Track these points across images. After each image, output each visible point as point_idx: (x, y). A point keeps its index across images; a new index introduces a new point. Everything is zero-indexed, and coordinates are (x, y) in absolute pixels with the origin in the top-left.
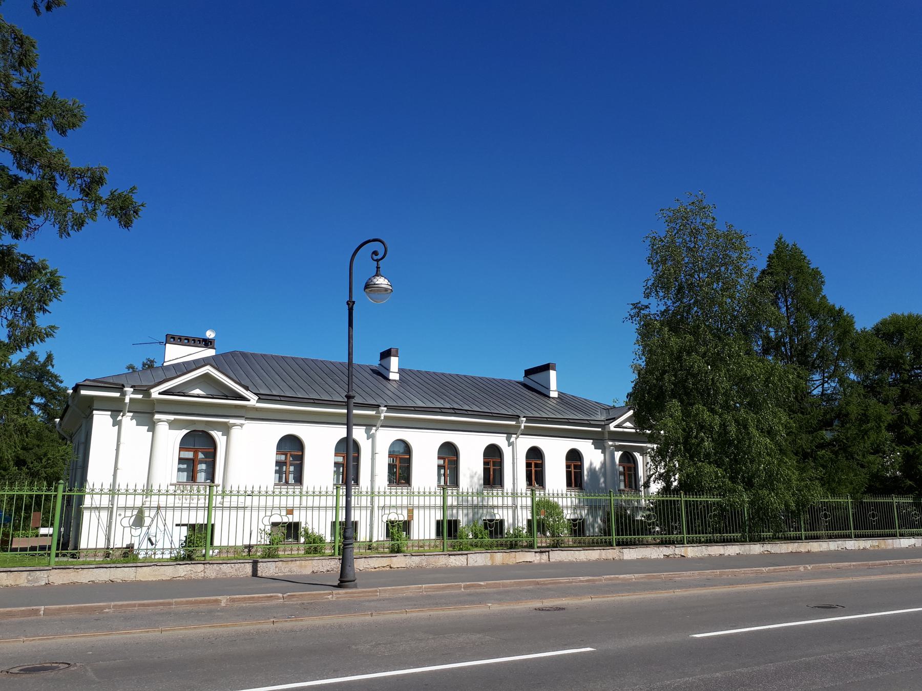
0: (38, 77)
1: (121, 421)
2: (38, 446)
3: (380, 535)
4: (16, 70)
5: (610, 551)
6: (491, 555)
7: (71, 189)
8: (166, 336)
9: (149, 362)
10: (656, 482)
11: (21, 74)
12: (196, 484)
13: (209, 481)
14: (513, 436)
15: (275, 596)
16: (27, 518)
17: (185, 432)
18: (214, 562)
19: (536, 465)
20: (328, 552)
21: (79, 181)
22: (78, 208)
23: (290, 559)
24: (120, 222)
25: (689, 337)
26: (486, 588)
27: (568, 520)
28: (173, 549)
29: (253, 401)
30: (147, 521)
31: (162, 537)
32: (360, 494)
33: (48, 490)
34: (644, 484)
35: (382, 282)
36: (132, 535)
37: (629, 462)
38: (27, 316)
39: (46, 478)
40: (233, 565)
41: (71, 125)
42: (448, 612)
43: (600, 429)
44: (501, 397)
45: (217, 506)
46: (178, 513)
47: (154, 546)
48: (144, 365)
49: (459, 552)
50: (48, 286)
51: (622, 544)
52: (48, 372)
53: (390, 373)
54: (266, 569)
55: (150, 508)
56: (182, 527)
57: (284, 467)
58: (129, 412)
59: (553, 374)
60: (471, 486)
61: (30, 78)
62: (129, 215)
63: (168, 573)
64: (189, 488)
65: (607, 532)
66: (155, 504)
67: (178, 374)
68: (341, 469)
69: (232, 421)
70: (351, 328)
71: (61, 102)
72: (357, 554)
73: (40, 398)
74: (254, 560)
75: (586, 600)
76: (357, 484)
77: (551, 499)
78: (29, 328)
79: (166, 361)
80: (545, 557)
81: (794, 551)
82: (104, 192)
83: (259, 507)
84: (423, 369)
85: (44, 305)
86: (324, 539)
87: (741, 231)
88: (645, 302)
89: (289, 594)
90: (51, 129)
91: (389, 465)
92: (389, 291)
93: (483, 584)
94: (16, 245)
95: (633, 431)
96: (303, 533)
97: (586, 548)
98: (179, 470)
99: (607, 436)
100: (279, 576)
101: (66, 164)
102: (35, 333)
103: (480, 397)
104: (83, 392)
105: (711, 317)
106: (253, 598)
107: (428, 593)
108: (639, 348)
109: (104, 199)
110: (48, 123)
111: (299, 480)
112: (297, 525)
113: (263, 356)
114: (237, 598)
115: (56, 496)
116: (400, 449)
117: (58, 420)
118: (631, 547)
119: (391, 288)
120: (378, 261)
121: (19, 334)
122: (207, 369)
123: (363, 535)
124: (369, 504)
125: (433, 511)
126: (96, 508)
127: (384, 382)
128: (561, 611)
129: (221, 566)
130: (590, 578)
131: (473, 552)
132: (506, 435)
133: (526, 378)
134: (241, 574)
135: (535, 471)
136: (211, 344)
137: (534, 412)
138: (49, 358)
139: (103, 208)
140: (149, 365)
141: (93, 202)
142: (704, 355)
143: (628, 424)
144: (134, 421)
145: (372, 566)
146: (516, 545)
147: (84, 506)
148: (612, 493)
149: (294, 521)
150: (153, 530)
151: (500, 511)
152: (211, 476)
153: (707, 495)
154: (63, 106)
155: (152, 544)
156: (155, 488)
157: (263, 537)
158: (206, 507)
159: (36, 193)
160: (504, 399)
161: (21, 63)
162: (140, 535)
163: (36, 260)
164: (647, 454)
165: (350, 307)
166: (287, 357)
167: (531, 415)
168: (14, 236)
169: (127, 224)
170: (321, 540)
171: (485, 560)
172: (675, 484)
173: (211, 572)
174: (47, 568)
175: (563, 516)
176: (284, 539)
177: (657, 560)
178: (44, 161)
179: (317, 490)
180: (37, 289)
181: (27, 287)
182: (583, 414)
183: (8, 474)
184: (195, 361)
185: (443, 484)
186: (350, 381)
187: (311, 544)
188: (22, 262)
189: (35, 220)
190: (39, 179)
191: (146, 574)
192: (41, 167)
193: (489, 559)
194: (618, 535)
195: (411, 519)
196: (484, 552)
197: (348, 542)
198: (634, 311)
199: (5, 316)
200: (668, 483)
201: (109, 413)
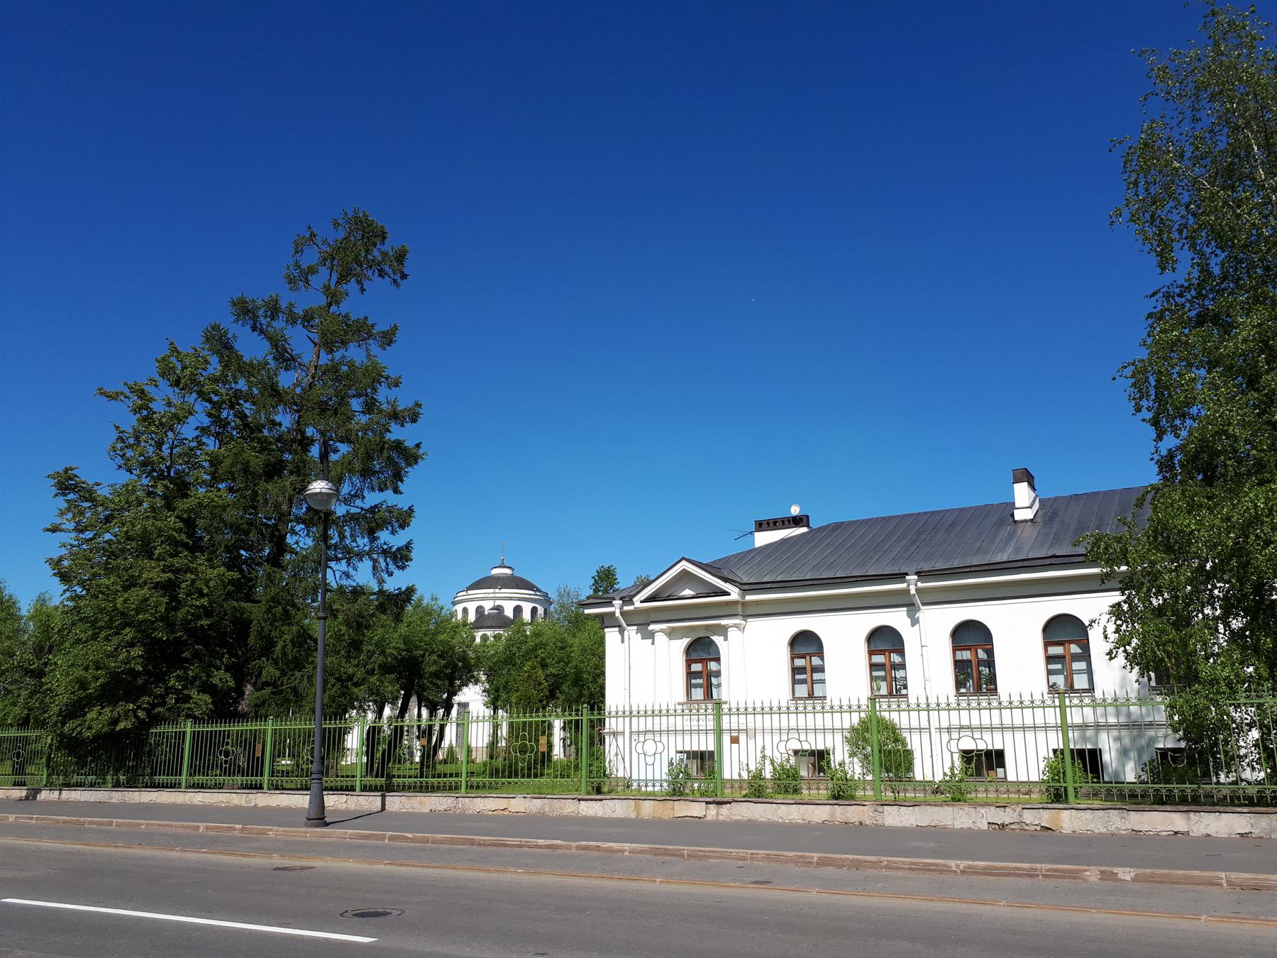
6: (635, 802)
17: (685, 641)
29: (735, 594)
36: (646, 764)
60: (1123, 686)
64: (704, 707)
69: (723, 622)
83: (780, 730)
87: (1122, 157)
125: (1041, 735)
149: (818, 748)
158: (1059, 727)
171: (627, 810)
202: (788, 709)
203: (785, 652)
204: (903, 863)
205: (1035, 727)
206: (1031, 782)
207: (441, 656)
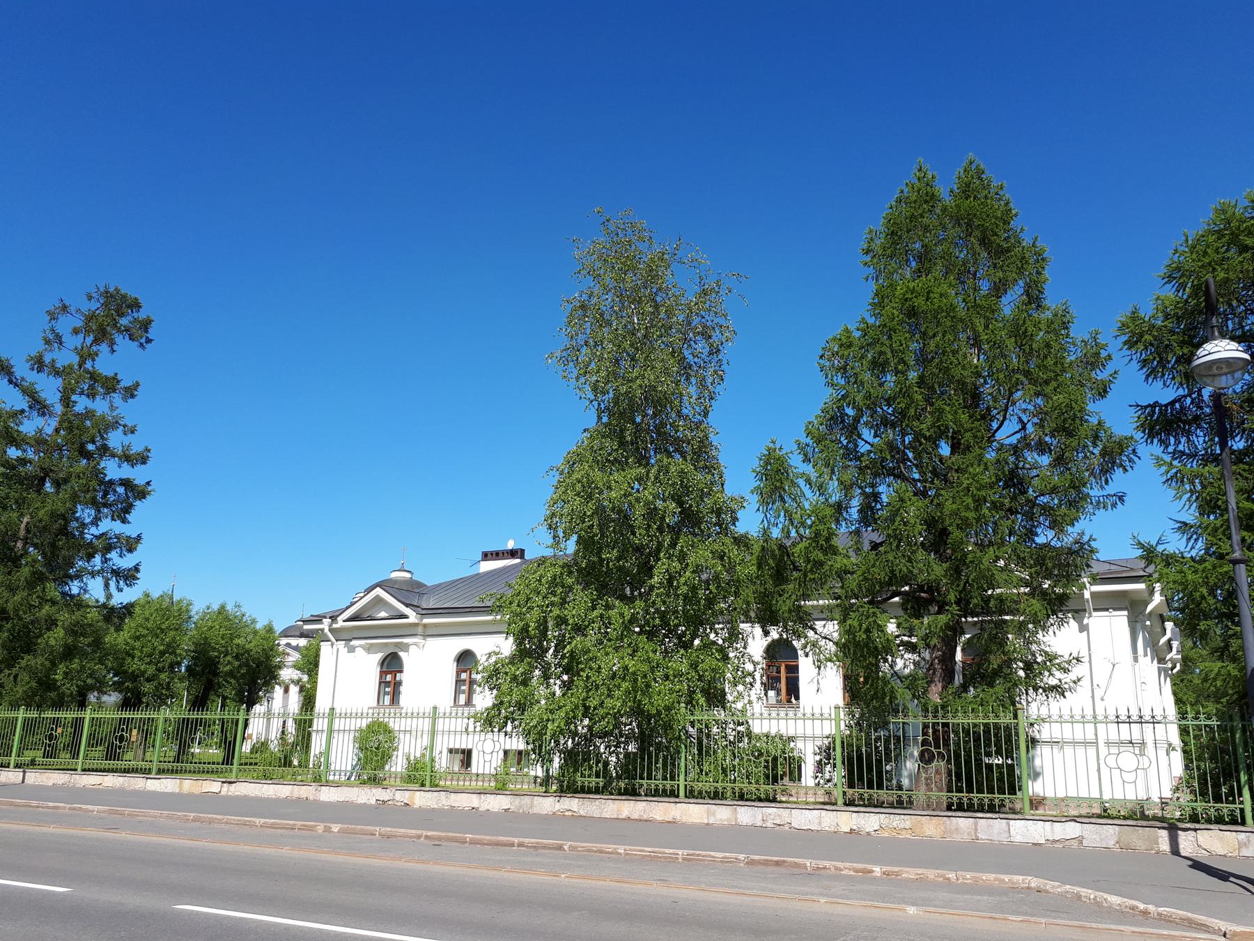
17: (378, 657)
29: (413, 617)
36: (1124, 781)
69: (406, 640)
81: (635, 816)
153: (122, 711)
177: (364, 806)
202: (761, 715)
203: (452, 668)
204: (234, 820)
207: (237, 657)
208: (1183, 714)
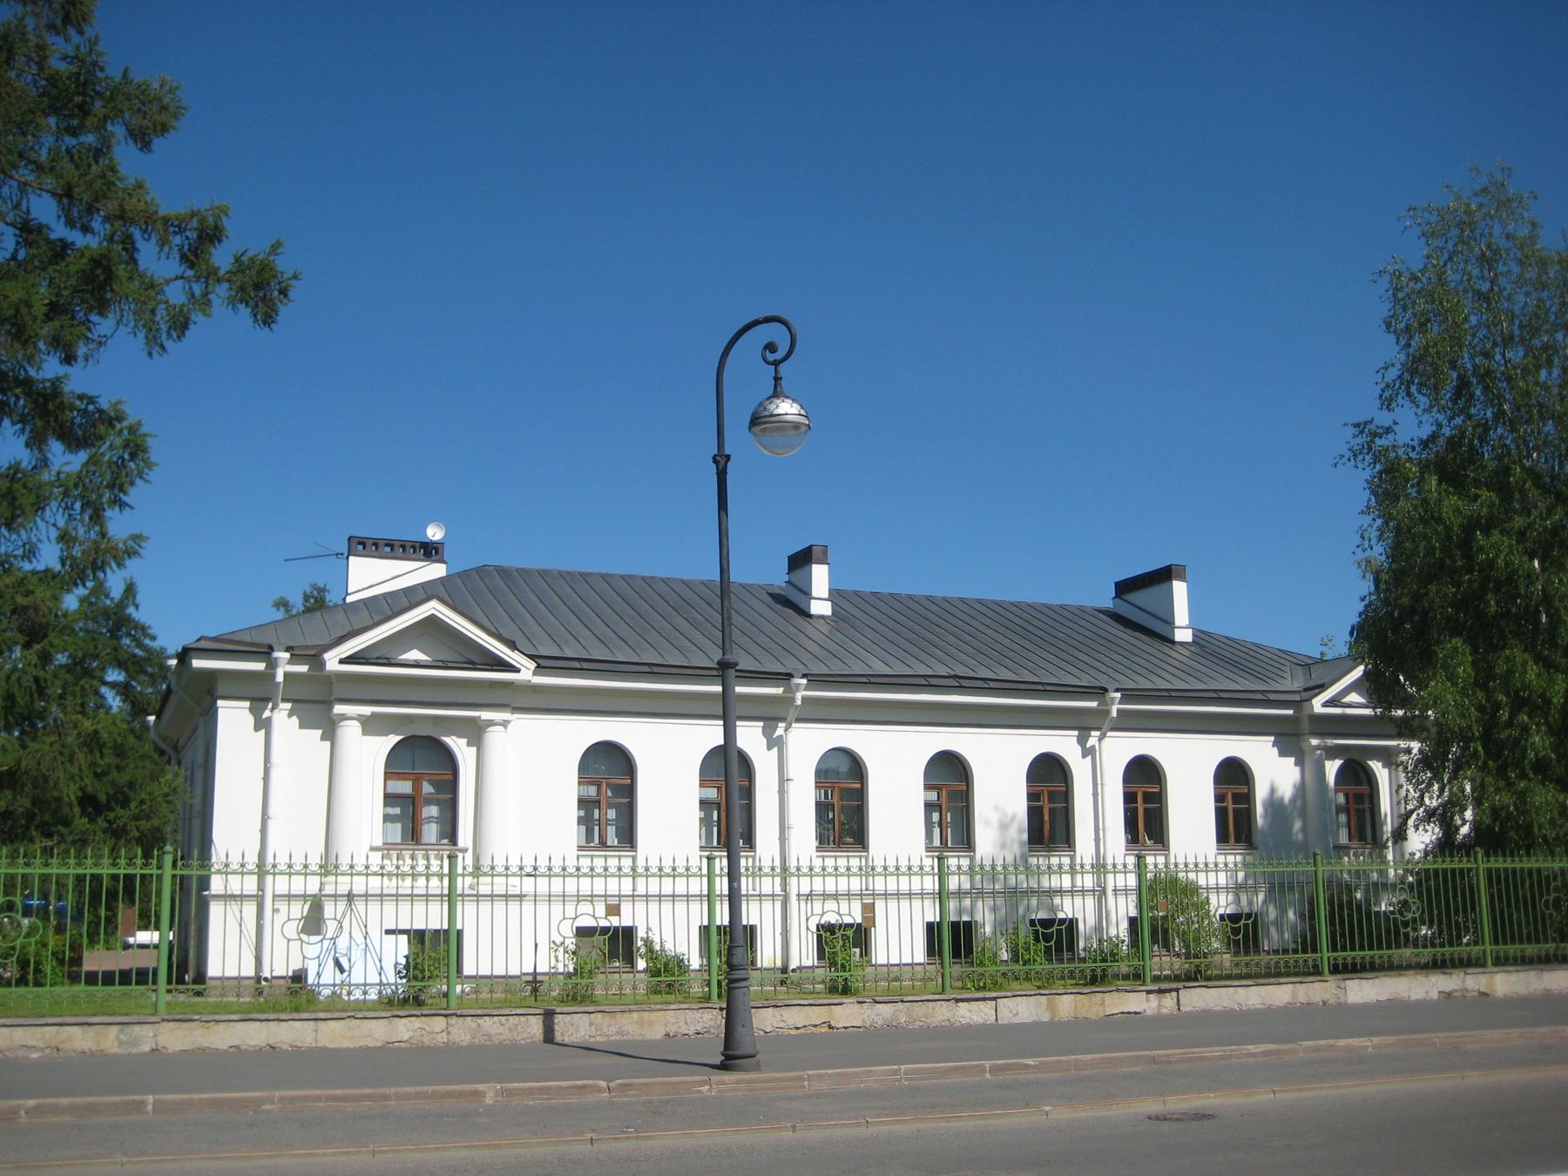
0: (96, 43)
1: (269, 719)
2: (118, 768)
3: (804, 953)
4: (58, 34)
5: (1316, 985)
7: (163, 256)
8: (349, 539)
9: (315, 593)
10: (1421, 828)
11: (67, 40)
12: (421, 847)
13: (445, 841)
14: (1093, 733)
15: (592, 1086)
16: (111, 920)
17: (394, 739)
18: (465, 1012)
19: (1148, 797)
20: (696, 990)
21: (177, 240)
22: (176, 294)
23: (619, 1008)
24: (255, 316)
25: (1485, 494)
26: (1040, 1072)
27: (1222, 917)
28: (384, 985)
29: (526, 672)
30: (331, 926)
31: (362, 959)
32: (757, 872)
33: (146, 865)
34: (1393, 833)
35: (787, 408)
36: (304, 957)
37: (1359, 782)
38: (91, 519)
39: (140, 841)
40: (503, 1019)
41: (159, 128)
42: (959, 1124)
43: (1290, 712)
44: (1062, 645)
45: (466, 892)
46: (389, 907)
47: (346, 974)
48: (306, 598)
49: (978, 995)
50: (126, 456)
51: (1344, 970)
52: (129, 619)
53: (812, 601)
54: (572, 1029)
55: (335, 897)
56: (394, 928)
57: (596, 812)
58: (284, 700)
59: (1179, 589)
60: (1003, 846)
61: (82, 48)
62: (271, 299)
63: (377, 1032)
65: (1308, 943)
66: (343, 889)
67: (377, 618)
68: (715, 813)
69: (486, 715)
70: (722, 513)
71: (139, 87)
72: (756, 993)
73: (116, 673)
74: (546, 1010)
75: (1262, 1098)
76: (751, 848)
77: (1181, 875)
78: (95, 542)
79: (349, 591)
80: (1169, 1001)
82: (222, 257)
84: (885, 588)
85: (121, 495)
86: (686, 963)
88: (1383, 419)
89: (620, 1081)
90: (123, 142)
91: (818, 804)
92: (804, 428)
93: (1032, 1063)
94: (66, 376)
95: (1367, 712)
96: (643, 950)
97: (1262, 981)
98: (387, 818)
99: (1306, 726)
100: (598, 1042)
101: (152, 209)
102: (107, 551)
103: (1014, 647)
104: (197, 663)
105: (1536, 448)
106: (549, 1088)
107: (914, 1083)
108: (1372, 523)
109: (222, 272)
110: (117, 130)
111: (628, 837)
112: (629, 932)
113: (543, 574)
114: (515, 1089)
115: (160, 877)
116: (844, 765)
117: (152, 718)
118: (1363, 975)
119: (807, 422)
120: (776, 363)
121: (79, 554)
122: (433, 608)
123: (768, 953)
124: (778, 890)
125: (917, 903)
126: (233, 897)
127: (799, 620)
128: (1206, 1123)
129: (480, 1021)
130: (1271, 1047)
131: (1009, 994)
132: (1076, 733)
133: (1118, 600)
134: (519, 1038)
135: (1145, 809)
136: (437, 553)
137: (1137, 678)
138: (130, 590)
139: (222, 290)
140: (316, 599)
141: (203, 280)
142: (1521, 535)
143: (1354, 697)
144: (295, 720)
145: (791, 1022)
146: (1104, 976)
147: (213, 893)
148: (1319, 857)
150: (343, 943)
151: (1067, 901)
152: (450, 832)
154: (143, 93)
155: (342, 971)
156: (344, 862)
157: (561, 957)
158: (445, 896)
159: (99, 272)
160: (1071, 650)
161: (67, 20)
162: (319, 957)
163: (104, 404)
164: (1398, 766)
165: (721, 466)
166: (590, 574)
167: (1133, 686)
168: (65, 359)
169: (268, 318)
170: (680, 964)
172: (1465, 830)
173: (462, 1032)
174: (153, 1019)
175: (1209, 911)
176: (604, 962)
177: (1422, 1005)
178: (112, 206)
179: (667, 864)
180: (108, 462)
181: (88, 462)
182: (1251, 678)
183: (71, 833)
184: (407, 591)
185: (939, 844)
186: (726, 622)
187: (660, 975)
188: (79, 411)
189: (99, 324)
190: (105, 243)
191: (335, 1034)
192: (107, 219)
193: (1044, 1007)
194: (1334, 949)
195: (871, 924)
196: (1033, 993)
197: (738, 974)
198: (1359, 440)
199: (52, 521)
200: (1449, 830)
201: (247, 704)
205: (910, 894)
206: (482, 977)
208: (131, 860)
